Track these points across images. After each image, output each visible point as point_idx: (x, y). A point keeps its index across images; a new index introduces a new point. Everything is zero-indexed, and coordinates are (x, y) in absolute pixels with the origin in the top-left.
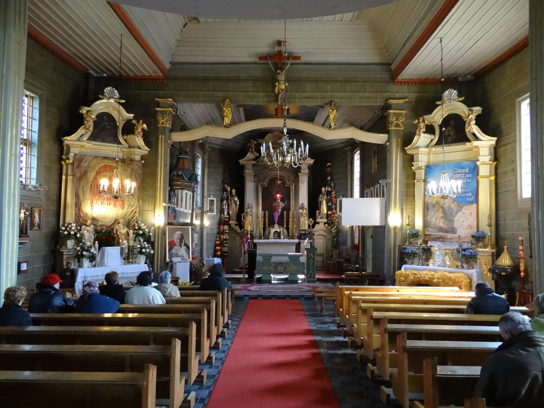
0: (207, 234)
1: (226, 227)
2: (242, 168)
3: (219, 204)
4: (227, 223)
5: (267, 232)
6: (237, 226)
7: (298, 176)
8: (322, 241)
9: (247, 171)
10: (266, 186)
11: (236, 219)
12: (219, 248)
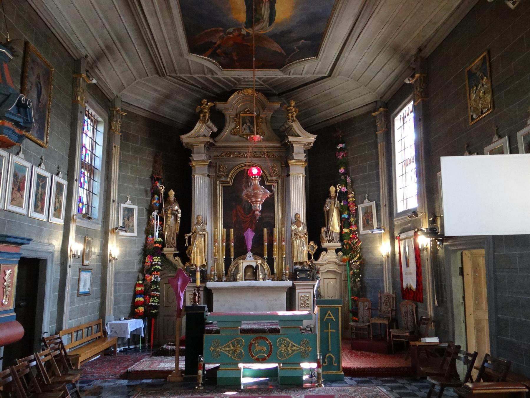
0: (116, 274)
1: (157, 259)
2: (186, 153)
3: (145, 218)
4: (158, 251)
5: (232, 268)
6: (177, 258)
7: (287, 166)
8: (332, 282)
9: (195, 157)
10: (231, 184)
11: (175, 245)
12: (142, 299)
